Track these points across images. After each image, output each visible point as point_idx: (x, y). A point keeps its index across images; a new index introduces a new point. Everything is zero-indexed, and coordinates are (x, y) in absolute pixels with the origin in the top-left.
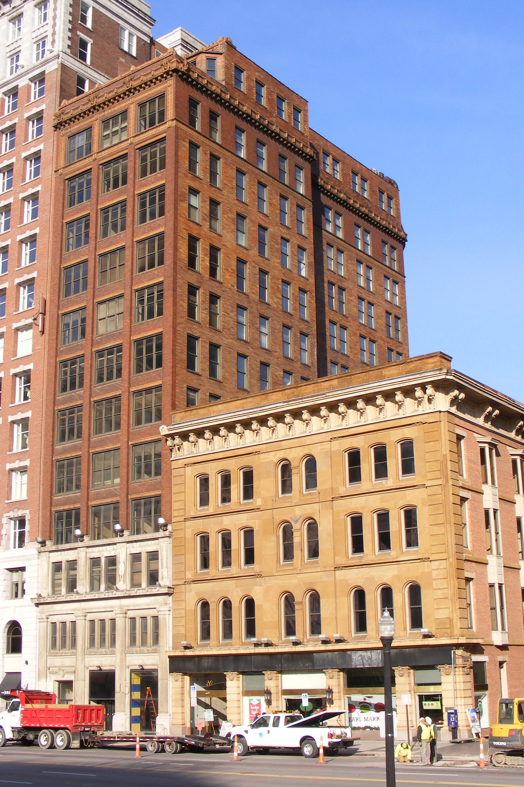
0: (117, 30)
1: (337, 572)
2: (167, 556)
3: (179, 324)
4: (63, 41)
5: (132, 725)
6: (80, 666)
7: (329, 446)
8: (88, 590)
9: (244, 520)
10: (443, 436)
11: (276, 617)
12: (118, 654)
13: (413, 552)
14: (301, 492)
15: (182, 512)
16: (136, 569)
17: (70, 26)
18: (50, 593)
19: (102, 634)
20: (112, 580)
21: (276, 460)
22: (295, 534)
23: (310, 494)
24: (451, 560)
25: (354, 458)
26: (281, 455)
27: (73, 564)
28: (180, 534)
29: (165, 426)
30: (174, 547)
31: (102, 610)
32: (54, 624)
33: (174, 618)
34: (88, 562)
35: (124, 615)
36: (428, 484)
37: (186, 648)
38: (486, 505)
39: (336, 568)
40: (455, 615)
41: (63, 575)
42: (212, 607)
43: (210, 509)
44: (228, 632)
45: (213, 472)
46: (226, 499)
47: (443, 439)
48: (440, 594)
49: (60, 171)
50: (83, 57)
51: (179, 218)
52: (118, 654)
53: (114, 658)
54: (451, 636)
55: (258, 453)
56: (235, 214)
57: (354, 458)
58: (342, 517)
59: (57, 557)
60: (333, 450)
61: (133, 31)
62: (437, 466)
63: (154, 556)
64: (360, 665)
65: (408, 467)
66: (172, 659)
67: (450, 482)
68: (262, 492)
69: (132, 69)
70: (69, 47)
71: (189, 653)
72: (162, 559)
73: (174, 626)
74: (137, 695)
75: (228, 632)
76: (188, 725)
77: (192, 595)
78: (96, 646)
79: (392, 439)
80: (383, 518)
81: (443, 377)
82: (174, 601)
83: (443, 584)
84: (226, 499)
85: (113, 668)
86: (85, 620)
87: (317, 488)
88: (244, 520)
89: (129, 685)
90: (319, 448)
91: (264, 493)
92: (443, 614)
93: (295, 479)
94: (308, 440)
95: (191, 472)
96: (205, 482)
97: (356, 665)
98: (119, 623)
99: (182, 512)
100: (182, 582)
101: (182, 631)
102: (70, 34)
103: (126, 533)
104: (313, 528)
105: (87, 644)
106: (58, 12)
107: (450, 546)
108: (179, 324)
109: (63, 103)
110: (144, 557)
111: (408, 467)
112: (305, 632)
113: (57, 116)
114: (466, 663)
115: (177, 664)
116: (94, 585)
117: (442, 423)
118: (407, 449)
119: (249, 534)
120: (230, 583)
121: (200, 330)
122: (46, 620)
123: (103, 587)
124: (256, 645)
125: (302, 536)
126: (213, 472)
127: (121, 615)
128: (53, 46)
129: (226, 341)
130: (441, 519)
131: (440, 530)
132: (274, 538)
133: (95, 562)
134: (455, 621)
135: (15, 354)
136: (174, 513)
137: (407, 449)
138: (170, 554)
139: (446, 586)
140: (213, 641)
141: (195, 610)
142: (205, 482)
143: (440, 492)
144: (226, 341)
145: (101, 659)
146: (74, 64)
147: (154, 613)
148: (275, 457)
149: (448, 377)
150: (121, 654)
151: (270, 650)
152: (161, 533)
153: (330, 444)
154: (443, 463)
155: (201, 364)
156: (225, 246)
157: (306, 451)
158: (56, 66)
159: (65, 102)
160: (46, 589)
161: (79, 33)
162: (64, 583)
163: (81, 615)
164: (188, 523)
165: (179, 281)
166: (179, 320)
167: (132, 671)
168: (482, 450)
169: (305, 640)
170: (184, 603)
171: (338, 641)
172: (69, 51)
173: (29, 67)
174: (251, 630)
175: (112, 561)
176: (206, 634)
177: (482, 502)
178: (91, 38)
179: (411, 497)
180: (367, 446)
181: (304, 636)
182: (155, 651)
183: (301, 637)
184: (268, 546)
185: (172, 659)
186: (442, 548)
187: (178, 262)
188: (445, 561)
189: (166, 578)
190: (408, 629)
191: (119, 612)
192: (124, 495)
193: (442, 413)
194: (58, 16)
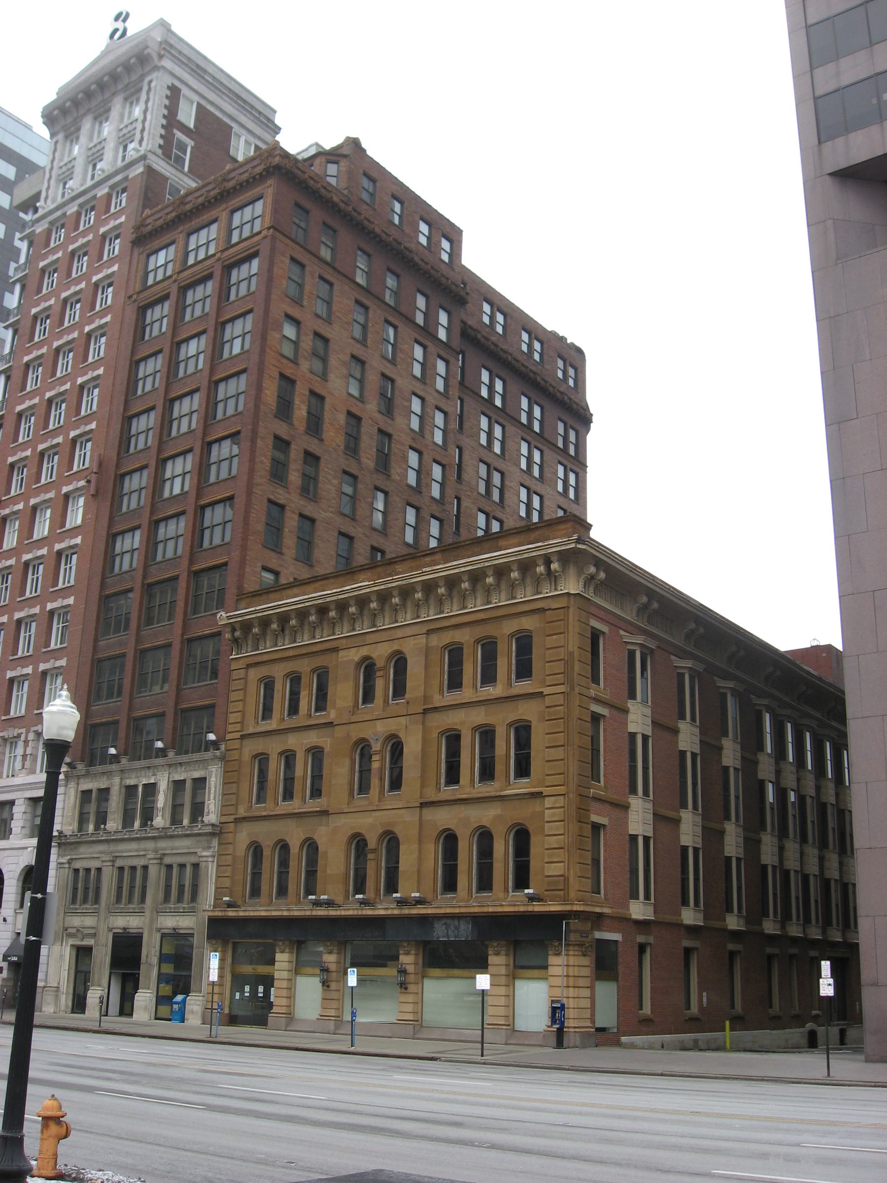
0: (226, 131)
1: (425, 811)
2: (216, 784)
3: (257, 485)
4: (153, 139)
5: (159, 1007)
6: (103, 928)
7: (425, 640)
8: (120, 827)
9: (312, 738)
10: (571, 627)
11: (342, 869)
12: (148, 913)
13: (522, 786)
14: (386, 701)
15: (238, 727)
16: (178, 802)
17: (164, 122)
18: (76, 829)
19: (131, 886)
20: (148, 816)
21: (356, 659)
22: (374, 758)
23: (397, 704)
24: (571, 795)
25: (456, 654)
26: (364, 651)
27: (104, 793)
28: (235, 755)
29: (223, 613)
30: (225, 772)
31: (132, 853)
32: (76, 871)
33: (219, 866)
34: (123, 790)
35: (158, 861)
36: (547, 691)
37: (230, 905)
38: (632, 728)
39: (423, 805)
40: (572, 872)
41: (92, 808)
42: (266, 853)
43: (272, 724)
44: (485, 882)
45: (278, 672)
46: (294, 709)
47: (571, 631)
48: (553, 842)
49: (135, 297)
50: (179, 161)
51: (268, 350)
52: (148, 913)
53: (143, 918)
54: (565, 900)
55: (336, 650)
56: (349, 356)
57: (456, 654)
58: (435, 735)
59: (86, 785)
60: (430, 645)
61: (252, 139)
62: (559, 667)
63: (200, 783)
64: (443, 937)
65: (524, 670)
66: (213, 921)
67: (577, 690)
68: (337, 701)
69: (227, 168)
70: (160, 146)
71: (231, 913)
72: (210, 788)
73: (218, 877)
74: (168, 969)
75: (485, 882)
76: (226, 1011)
77: (243, 837)
78: (124, 900)
79: (505, 632)
80: (487, 735)
81: (573, 546)
82: (220, 844)
83: (559, 828)
84: (294, 709)
85: (140, 931)
86: (113, 866)
87: (407, 696)
88: (312, 738)
89: (158, 954)
90: (412, 643)
91: (340, 703)
92: (556, 869)
93: (379, 684)
94: (399, 633)
95: (254, 675)
96: (269, 685)
97: (438, 937)
98: (153, 871)
99: (238, 727)
100: (231, 818)
101: (227, 882)
102: (163, 132)
103: (171, 754)
104: (397, 749)
105: (113, 899)
106: (150, 104)
107: (571, 776)
108: (257, 485)
109: (145, 213)
110: (189, 785)
111: (524, 670)
112: (377, 890)
113: (137, 228)
114: (584, 939)
115: (221, 930)
116: (127, 821)
117: (571, 610)
118: (524, 643)
119: (316, 753)
120: (291, 824)
121: (287, 496)
122: (67, 866)
123: (137, 824)
124: (317, 904)
125: (383, 760)
126: (278, 672)
127: (155, 861)
128: (141, 146)
129: (324, 515)
130: (561, 738)
131: (559, 753)
132: (347, 762)
133: (131, 790)
134: (571, 879)
135: (63, 524)
136: (230, 728)
137: (524, 643)
138: (220, 781)
139: (561, 832)
140: (264, 898)
141: (246, 857)
142: (269, 685)
143: (562, 703)
144: (324, 515)
145: (128, 918)
146: (162, 166)
147: (193, 859)
148: (355, 655)
149: (580, 546)
150: (152, 913)
151: (332, 913)
152: (209, 755)
153: (427, 639)
154: (568, 662)
155: (290, 541)
156: (332, 394)
157: (395, 647)
158: (141, 170)
159: (148, 212)
160: (71, 825)
161: (175, 131)
162: (92, 818)
163: (108, 859)
164: (246, 742)
165: (262, 431)
166: (258, 480)
167: (163, 936)
168: (632, 654)
169: (378, 900)
170: (231, 846)
171: (419, 902)
172: (160, 152)
173: (111, 171)
174: (522, 880)
175: (151, 789)
176: (450, 885)
177: (626, 724)
178: (193, 140)
179: (527, 711)
180: (472, 640)
181: (376, 894)
182: (192, 911)
183: (373, 896)
184: (340, 773)
185: (213, 921)
186: (559, 779)
187: (262, 407)
188: (562, 797)
189: (212, 815)
190: (510, 890)
191: (152, 856)
192: (171, 704)
193: (572, 598)
194: (150, 109)
